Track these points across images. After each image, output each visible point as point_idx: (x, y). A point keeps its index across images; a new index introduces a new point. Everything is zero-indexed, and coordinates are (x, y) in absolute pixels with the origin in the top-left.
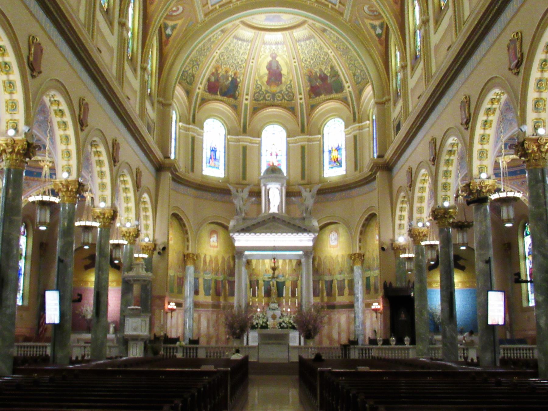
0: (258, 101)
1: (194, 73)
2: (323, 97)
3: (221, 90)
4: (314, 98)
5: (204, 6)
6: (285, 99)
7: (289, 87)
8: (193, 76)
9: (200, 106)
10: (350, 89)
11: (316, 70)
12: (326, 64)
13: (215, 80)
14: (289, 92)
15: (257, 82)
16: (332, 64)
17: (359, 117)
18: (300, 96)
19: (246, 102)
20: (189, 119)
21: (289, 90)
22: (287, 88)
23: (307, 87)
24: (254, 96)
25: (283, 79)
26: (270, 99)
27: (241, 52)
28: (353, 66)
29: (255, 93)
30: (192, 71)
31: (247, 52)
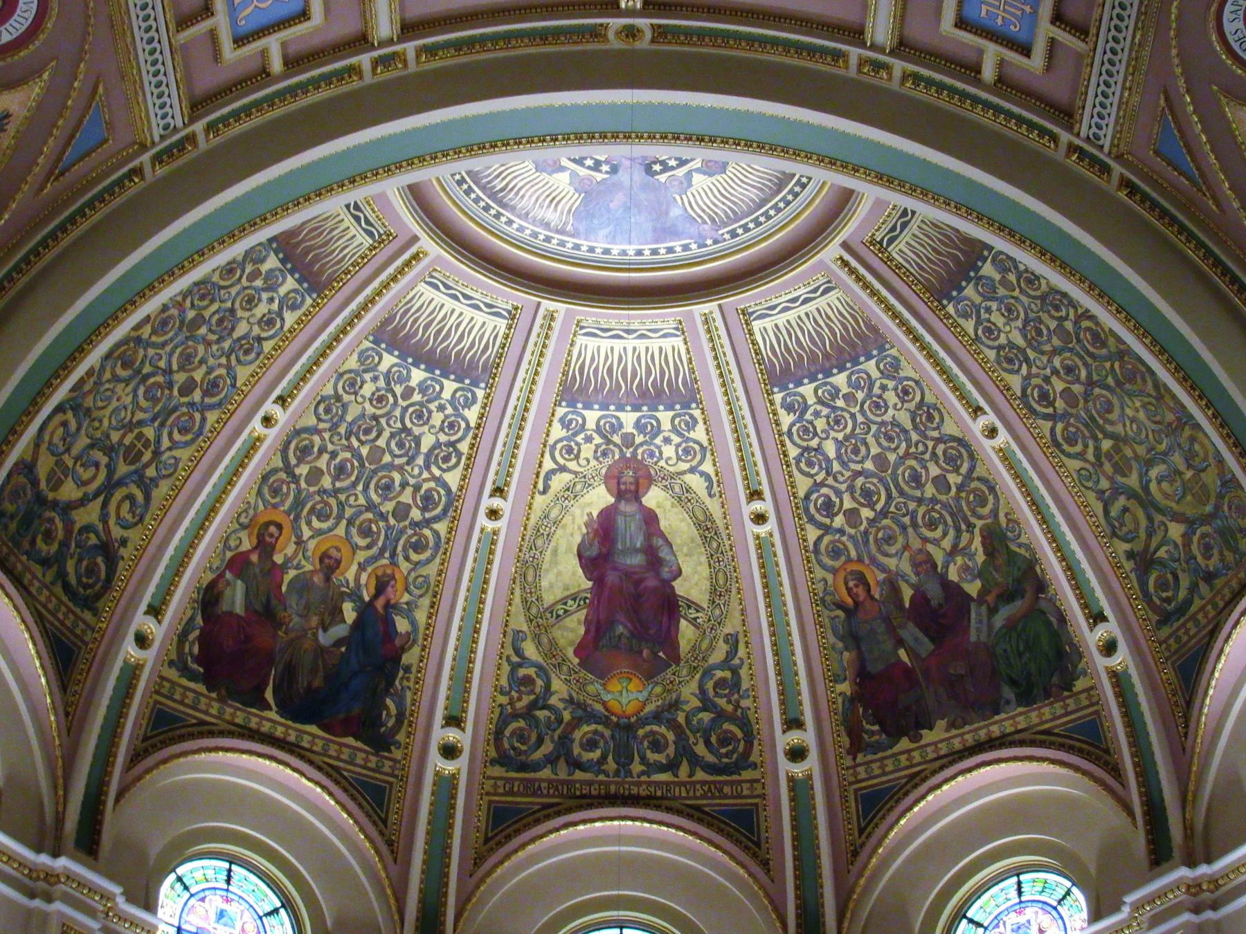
0: (523, 767)
1: (117, 532)
2: (936, 735)
3: (289, 673)
4: (877, 748)
5: (184, 22)
6: (695, 761)
7: (721, 683)
8: (108, 550)
9: (136, 757)
10: (1122, 658)
11: (892, 563)
12: (961, 522)
13: (248, 605)
14: (721, 715)
15: (518, 652)
16: (995, 513)
17: (1188, 829)
18: (795, 737)
19: (449, 767)
20: (60, 820)
21: (722, 702)
22: (710, 685)
23: (837, 679)
24: (498, 734)
25: (686, 633)
26: (604, 758)
27: (427, 442)
28: (1132, 504)
29: (504, 720)
30: (104, 518)
31: (464, 447)
